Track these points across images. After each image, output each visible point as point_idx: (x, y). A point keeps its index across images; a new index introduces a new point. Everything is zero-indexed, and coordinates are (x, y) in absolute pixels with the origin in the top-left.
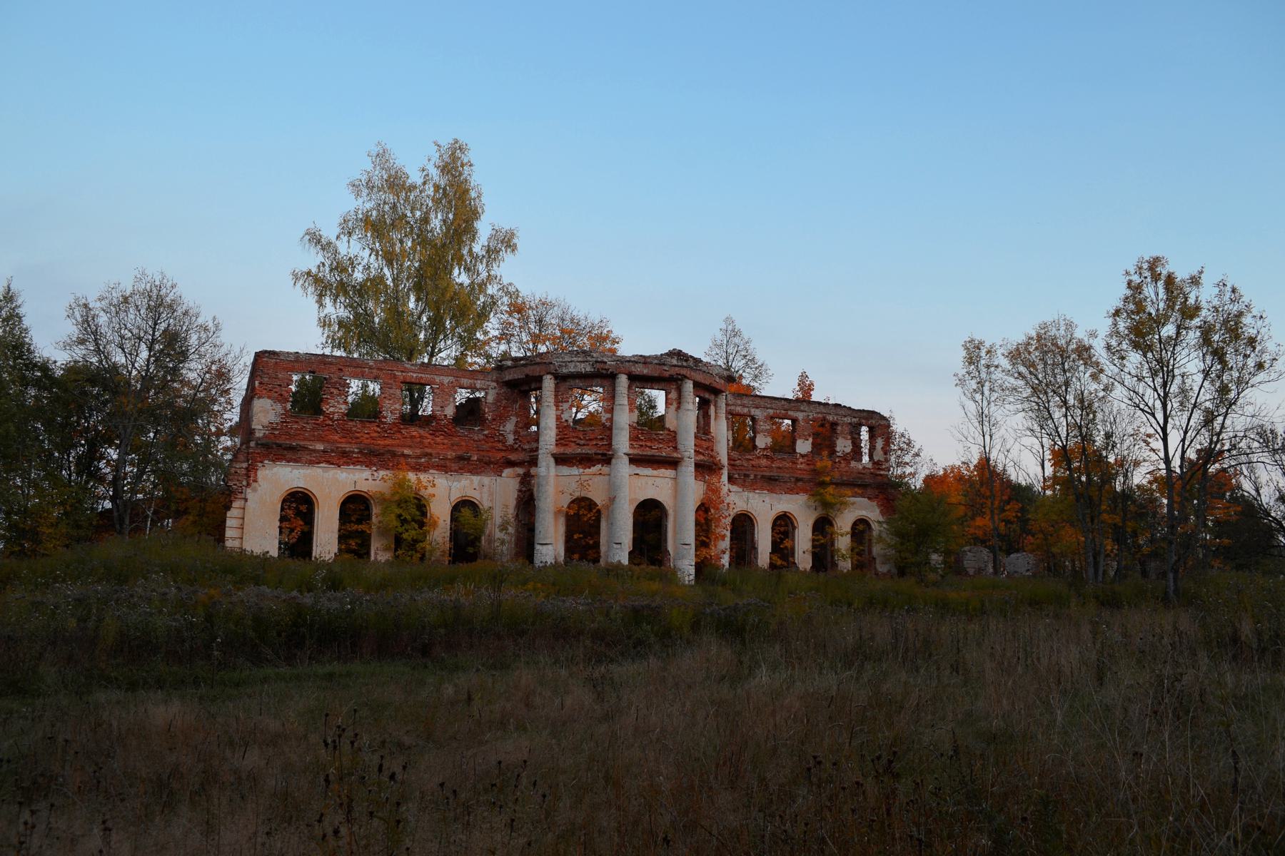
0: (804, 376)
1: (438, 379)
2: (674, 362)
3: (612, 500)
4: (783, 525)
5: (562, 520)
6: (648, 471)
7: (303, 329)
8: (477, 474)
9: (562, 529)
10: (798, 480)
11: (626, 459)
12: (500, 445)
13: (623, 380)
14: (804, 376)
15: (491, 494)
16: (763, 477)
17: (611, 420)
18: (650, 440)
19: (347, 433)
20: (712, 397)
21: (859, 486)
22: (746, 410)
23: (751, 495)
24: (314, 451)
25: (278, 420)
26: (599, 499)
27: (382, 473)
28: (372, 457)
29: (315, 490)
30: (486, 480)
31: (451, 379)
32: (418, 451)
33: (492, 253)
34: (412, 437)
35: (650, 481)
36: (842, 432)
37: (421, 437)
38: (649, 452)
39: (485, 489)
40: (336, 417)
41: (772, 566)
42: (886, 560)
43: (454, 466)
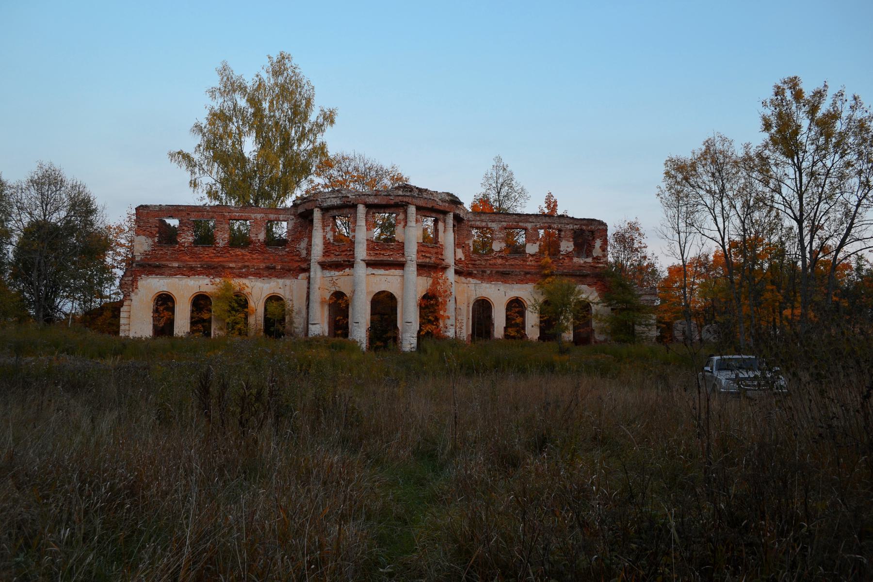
0: (550, 196)
1: (253, 216)
2: (400, 193)
3: (354, 292)
4: (516, 307)
5: (326, 308)
6: (382, 271)
7: (184, 189)
8: (282, 278)
9: (326, 313)
10: (526, 273)
11: (363, 265)
12: (297, 258)
13: (361, 209)
14: (550, 196)
15: (291, 291)
16: (497, 272)
17: (354, 236)
18: (384, 249)
19: (194, 255)
20: (442, 216)
21: (579, 276)
22: (484, 224)
23: (488, 285)
24: (172, 267)
25: (150, 249)
26: (347, 291)
27: (218, 280)
28: (210, 270)
29: (174, 293)
30: (288, 282)
31: (262, 215)
32: (240, 265)
33: (320, 127)
34: (237, 255)
35: (384, 278)
36: (565, 236)
37: (243, 255)
38: (381, 258)
39: (287, 288)
40: (186, 245)
41: (507, 336)
42: (602, 331)
43: (266, 273)
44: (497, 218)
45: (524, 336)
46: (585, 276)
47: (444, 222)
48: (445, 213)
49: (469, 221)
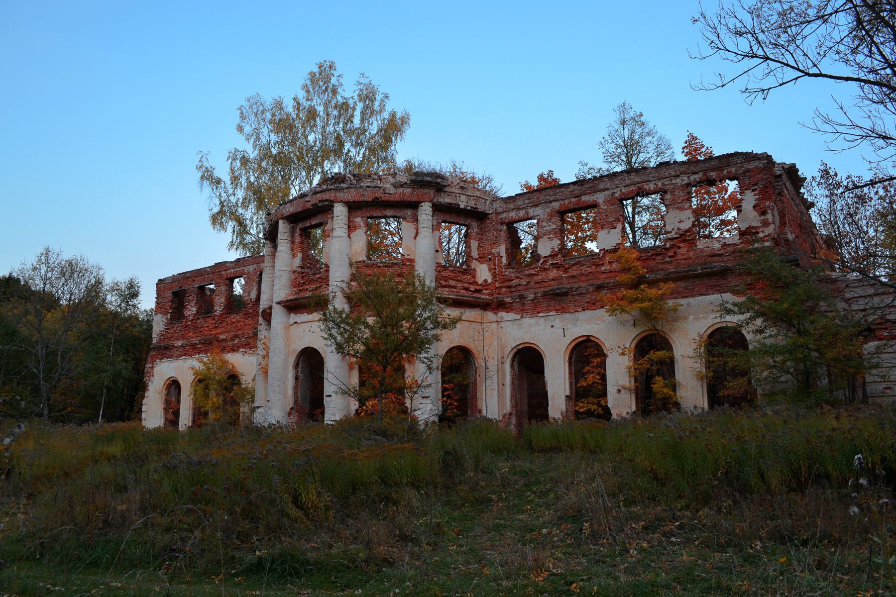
1: (246, 269)
4: (586, 355)
21: (709, 275)
23: (533, 321)
31: (255, 266)
35: (307, 327)
44: (542, 197)
45: (607, 412)
46: (723, 273)
47: (416, 220)
48: (414, 206)
49: (498, 214)
